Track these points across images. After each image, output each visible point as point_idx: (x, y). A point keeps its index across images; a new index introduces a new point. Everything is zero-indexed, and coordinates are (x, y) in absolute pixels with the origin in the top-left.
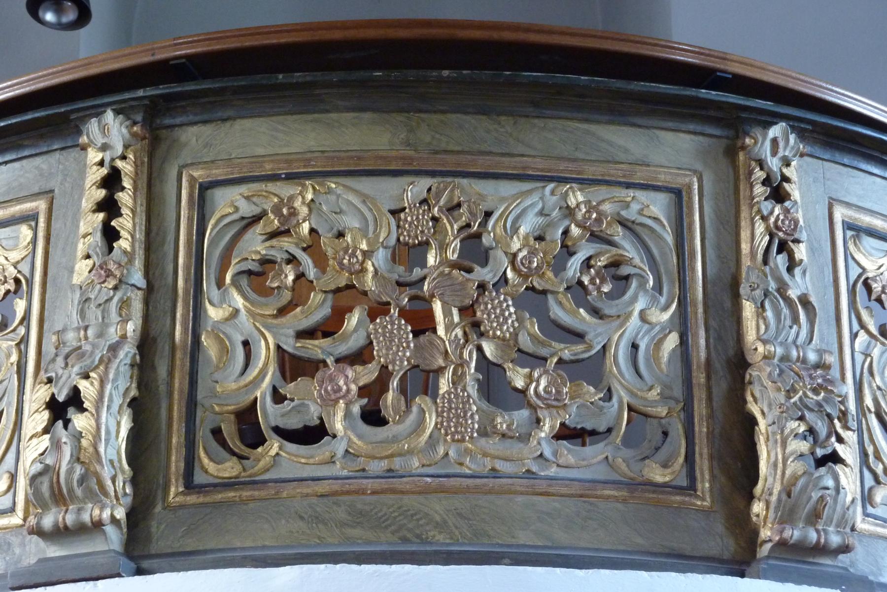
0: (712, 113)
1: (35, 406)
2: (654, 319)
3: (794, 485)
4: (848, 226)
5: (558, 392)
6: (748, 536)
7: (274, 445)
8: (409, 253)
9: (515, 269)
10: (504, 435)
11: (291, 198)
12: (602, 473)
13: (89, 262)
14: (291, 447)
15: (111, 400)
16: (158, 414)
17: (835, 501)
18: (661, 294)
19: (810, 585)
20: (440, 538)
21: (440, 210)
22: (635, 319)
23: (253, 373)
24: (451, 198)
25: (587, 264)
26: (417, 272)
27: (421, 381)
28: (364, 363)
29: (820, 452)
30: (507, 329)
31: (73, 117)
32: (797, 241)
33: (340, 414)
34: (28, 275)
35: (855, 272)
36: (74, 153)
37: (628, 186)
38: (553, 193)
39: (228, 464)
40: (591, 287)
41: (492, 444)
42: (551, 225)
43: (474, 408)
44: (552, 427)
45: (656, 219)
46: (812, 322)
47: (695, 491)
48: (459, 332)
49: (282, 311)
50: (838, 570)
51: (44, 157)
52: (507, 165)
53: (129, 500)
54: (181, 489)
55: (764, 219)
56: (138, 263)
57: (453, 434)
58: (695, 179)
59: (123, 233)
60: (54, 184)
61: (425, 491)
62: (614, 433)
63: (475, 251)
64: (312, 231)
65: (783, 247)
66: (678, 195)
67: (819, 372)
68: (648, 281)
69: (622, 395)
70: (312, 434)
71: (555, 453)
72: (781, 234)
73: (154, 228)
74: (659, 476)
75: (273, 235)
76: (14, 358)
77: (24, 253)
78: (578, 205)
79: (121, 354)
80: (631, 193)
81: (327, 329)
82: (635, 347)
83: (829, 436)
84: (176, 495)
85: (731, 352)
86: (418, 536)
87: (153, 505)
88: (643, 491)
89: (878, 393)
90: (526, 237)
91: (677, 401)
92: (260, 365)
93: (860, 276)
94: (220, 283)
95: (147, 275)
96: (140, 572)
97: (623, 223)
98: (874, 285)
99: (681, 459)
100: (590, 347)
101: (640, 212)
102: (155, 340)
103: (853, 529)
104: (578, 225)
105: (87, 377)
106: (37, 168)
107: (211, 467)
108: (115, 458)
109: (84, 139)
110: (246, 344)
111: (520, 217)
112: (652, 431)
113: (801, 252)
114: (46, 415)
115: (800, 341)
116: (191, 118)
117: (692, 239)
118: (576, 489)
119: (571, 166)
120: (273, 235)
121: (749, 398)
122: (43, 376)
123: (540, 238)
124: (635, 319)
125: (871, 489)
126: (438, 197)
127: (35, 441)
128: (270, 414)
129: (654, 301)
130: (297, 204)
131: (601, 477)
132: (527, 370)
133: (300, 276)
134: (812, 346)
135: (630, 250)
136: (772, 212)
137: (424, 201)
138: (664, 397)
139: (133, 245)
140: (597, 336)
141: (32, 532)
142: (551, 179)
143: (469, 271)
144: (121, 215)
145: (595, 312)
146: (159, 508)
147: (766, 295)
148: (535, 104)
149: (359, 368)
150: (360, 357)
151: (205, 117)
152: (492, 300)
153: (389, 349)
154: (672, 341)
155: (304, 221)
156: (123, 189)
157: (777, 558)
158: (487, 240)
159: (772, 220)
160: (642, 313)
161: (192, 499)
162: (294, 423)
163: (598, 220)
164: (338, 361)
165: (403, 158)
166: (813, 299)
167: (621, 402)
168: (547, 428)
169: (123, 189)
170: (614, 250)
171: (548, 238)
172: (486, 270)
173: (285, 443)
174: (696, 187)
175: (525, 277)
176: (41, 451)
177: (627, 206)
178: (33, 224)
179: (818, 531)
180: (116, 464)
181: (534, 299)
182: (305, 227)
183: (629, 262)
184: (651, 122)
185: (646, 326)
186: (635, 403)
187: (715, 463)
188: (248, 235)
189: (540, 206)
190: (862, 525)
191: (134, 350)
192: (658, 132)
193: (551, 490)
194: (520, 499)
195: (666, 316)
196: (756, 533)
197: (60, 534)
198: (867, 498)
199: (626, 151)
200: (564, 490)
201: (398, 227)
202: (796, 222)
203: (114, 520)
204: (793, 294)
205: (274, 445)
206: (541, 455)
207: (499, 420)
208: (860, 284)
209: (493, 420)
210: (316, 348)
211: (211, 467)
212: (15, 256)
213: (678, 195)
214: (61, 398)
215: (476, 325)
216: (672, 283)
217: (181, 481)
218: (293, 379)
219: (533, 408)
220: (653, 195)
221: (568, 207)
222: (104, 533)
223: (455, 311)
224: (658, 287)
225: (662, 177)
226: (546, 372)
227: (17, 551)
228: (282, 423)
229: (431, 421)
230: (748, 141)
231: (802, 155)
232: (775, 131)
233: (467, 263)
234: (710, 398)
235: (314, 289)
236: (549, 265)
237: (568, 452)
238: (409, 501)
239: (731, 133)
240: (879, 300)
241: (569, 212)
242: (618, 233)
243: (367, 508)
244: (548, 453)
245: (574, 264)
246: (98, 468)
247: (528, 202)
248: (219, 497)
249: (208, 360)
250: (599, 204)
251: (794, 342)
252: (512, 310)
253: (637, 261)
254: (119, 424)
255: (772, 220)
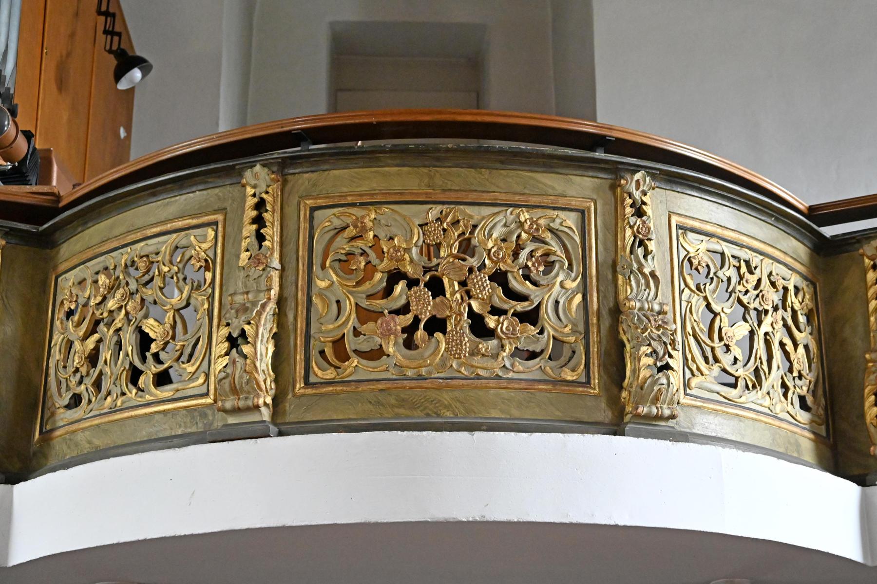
0: (602, 166)
1: (220, 339)
2: (567, 286)
3: (645, 382)
4: (679, 227)
5: (514, 330)
6: (620, 411)
7: (355, 361)
8: (432, 249)
9: (490, 258)
10: (483, 355)
11: (363, 217)
12: (538, 376)
13: (248, 253)
14: (364, 362)
15: (263, 336)
16: (289, 342)
17: (667, 391)
18: (572, 271)
19: (652, 438)
20: (448, 414)
21: (447, 225)
22: (557, 287)
23: (342, 319)
24: (454, 218)
25: (531, 255)
26: (435, 261)
27: (436, 325)
28: (404, 314)
29: (659, 364)
30: (485, 294)
31: (237, 167)
32: (650, 240)
33: (392, 344)
34: (212, 257)
35: (683, 254)
36: (238, 187)
37: (554, 209)
38: (511, 214)
39: (329, 371)
40: (532, 268)
41: (477, 360)
42: (511, 233)
43: (467, 339)
44: (510, 350)
45: (570, 228)
46: (657, 288)
47: (590, 384)
48: (458, 296)
49: (359, 283)
50: (668, 429)
51: (221, 189)
52: (486, 198)
53: (273, 392)
54: (302, 385)
55: (631, 227)
56: (276, 255)
57: (454, 355)
58: (592, 204)
59: (267, 237)
60: (227, 205)
61: (439, 388)
62: (545, 353)
63: (467, 248)
64: (375, 236)
65: (641, 243)
66: (583, 213)
67: (660, 317)
68: (564, 264)
69: (550, 331)
70: (377, 354)
71: (513, 365)
72: (640, 236)
73: (285, 234)
74: (569, 376)
75: (353, 239)
76: (206, 306)
77: (210, 244)
78: (526, 221)
79: (268, 309)
80: (556, 213)
81: (388, 292)
82: (557, 302)
83: (664, 355)
84: (300, 389)
85: (611, 305)
86: (435, 413)
87: (286, 394)
88: (561, 385)
89: (695, 324)
90: (496, 240)
91: (581, 333)
92: (346, 314)
93: (685, 257)
94: (323, 267)
95: (281, 262)
96: (281, 434)
97: (551, 230)
98: (694, 261)
99: (582, 367)
100: (533, 303)
101: (561, 224)
102: (286, 299)
103: (678, 403)
104: (526, 232)
105: (249, 323)
106: (216, 195)
107: (319, 373)
108: (265, 368)
109: (244, 181)
110: (338, 302)
111: (493, 228)
112: (567, 352)
113: (651, 246)
114: (226, 344)
115: (649, 299)
116: (305, 169)
117: (590, 239)
118: (523, 385)
119: (522, 198)
120: (353, 239)
121: (621, 331)
122: (224, 322)
123: (504, 240)
124: (557, 287)
125: (689, 379)
126: (447, 216)
127: (220, 360)
128: (350, 344)
129: (568, 275)
130: (366, 220)
131: (538, 378)
132: (497, 317)
133: (368, 263)
134: (657, 301)
135: (555, 247)
136: (635, 224)
137: (438, 219)
138: (574, 332)
139: (273, 245)
140: (536, 297)
141: (219, 410)
142: (510, 206)
143: (464, 260)
144: (266, 226)
145: (535, 284)
146: (290, 396)
147: (631, 273)
148: (502, 162)
149: (401, 317)
150: (404, 310)
151: (313, 169)
152: (476, 277)
153: (417, 305)
154: (579, 298)
155: (370, 230)
156: (267, 211)
157: (634, 423)
158: (475, 242)
159: (636, 228)
160: (561, 283)
161: (309, 391)
162: (365, 347)
163: (537, 230)
164: (390, 313)
165: (426, 194)
166: (657, 274)
167: (549, 332)
168: (507, 351)
169: (267, 211)
170: (546, 247)
171: (508, 240)
172: (473, 260)
173: (361, 360)
174: (593, 208)
175: (496, 263)
176: (224, 364)
177: (554, 220)
178: (215, 227)
179: (657, 408)
180: (266, 372)
181: (499, 278)
182: (371, 234)
183: (554, 253)
184: (567, 171)
185: (564, 291)
186: (556, 335)
187: (601, 368)
188: (339, 239)
189: (504, 221)
190: (684, 400)
191: (275, 306)
192: (571, 177)
193: (509, 386)
194: (492, 391)
195: (575, 284)
196: (624, 408)
197: (236, 411)
198: (687, 385)
199: (553, 188)
200: (517, 386)
201: (424, 234)
202: (649, 229)
203: (265, 404)
204: (647, 271)
205: (355, 361)
206: (504, 366)
207: (480, 346)
208: (686, 260)
209: (478, 346)
210: (379, 304)
211: (319, 373)
212: (205, 246)
213: (583, 213)
214: (235, 335)
215: (468, 293)
216: (578, 266)
217: (302, 381)
218: (365, 323)
219: (500, 339)
220: (568, 213)
221: (520, 222)
222: (260, 411)
223: (456, 284)
224: (570, 265)
225: (574, 203)
226: (507, 318)
227: (211, 418)
228: (359, 348)
229: (443, 346)
230: (623, 182)
231: (653, 189)
232: (638, 176)
233: (462, 255)
234: (599, 331)
235: (376, 271)
236: (509, 256)
237: (520, 365)
238: (432, 394)
239: (613, 177)
240: (697, 269)
241: (521, 225)
242: (548, 236)
243: (407, 397)
244: (508, 365)
245: (524, 254)
246: (256, 375)
247: (497, 219)
248: (324, 390)
249: (317, 310)
250: (537, 220)
251: (647, 299)
252: (488, 282)
253: (559, 253)
254: (267, 349)
255: (636, 228)
